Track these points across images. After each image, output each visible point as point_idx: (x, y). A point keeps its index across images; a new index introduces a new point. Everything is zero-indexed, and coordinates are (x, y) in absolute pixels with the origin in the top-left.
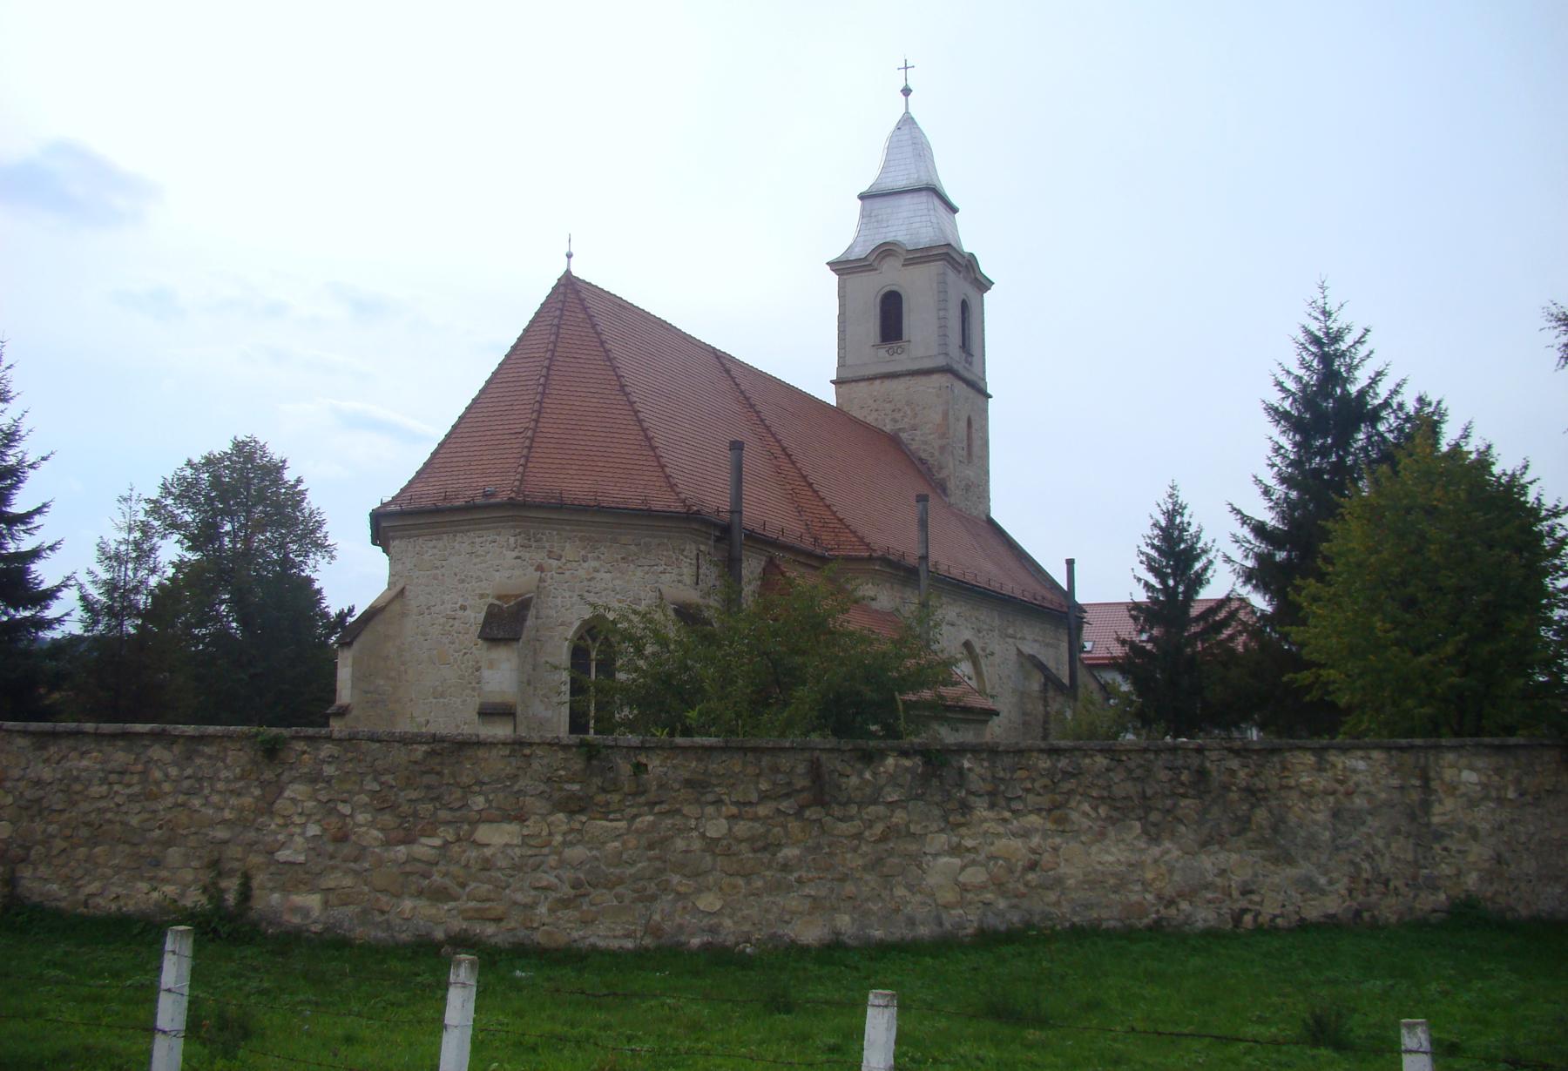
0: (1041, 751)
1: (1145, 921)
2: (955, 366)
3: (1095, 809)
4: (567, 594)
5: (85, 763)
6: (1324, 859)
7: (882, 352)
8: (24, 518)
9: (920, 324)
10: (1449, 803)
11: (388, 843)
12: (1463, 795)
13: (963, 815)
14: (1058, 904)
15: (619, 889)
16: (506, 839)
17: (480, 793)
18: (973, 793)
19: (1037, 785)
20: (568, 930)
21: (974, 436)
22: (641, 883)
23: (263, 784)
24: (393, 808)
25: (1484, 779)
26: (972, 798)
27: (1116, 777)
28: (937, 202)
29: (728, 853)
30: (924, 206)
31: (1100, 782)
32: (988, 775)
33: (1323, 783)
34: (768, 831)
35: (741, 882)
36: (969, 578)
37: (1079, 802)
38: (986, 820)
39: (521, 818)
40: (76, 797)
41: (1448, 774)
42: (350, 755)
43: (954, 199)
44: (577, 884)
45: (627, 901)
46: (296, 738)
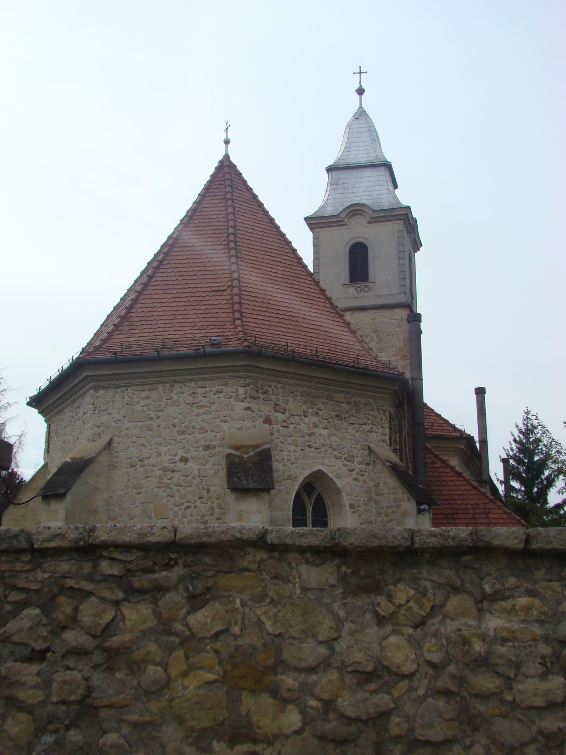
4: (292, 448)
5: (494, 623)
9: (381, 267)
28: (388, 174)
40: (481, 707)
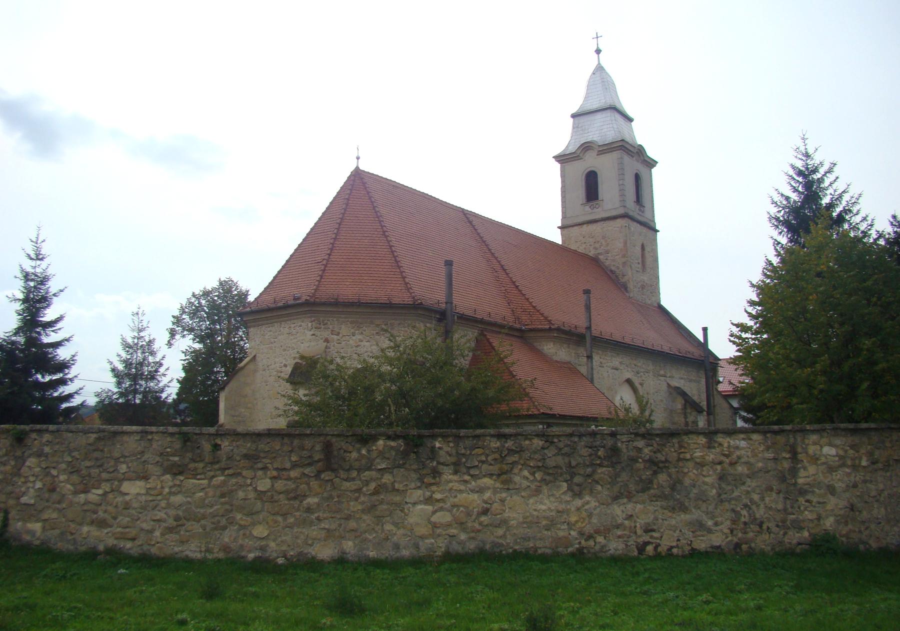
0: (492, 436)
1: (570, 550)
2: (631, 213)
3: (533, 474)
6: (711, 508)
7: (587, 208)
8: (51, 324)
9: (608, 190)
10: (812, 470)
11: (76, 493)
12: (824, 463)
13: (434, 478)
14: (504, 536)
15: (203, 522)
16: (137, 490)
17: (123, 463)
18: (443, 464)
19: (489, 458)
20: (170, 546)
21: (647, 255)
22: (217, 518)
23: (16, 458)
24: (78, 471)
25: (841, 453)
26: (441, 467)
27: (549, 453)
28: (618, 116)
29: (272, 501)
30: (609, 119)
31: (537, 456)
32: (454, 452)
33: (712, 456)
34: (298, 487)
35: (280, 519)
36: (627, 340)
37: (521, 469)
38: (451, 481)
39: (146, 478)
41: (812, 449)
42: (57, 440)
43: (630, 113)
44: (177, 518)
45: (208, 529)
46: (32, 431)
